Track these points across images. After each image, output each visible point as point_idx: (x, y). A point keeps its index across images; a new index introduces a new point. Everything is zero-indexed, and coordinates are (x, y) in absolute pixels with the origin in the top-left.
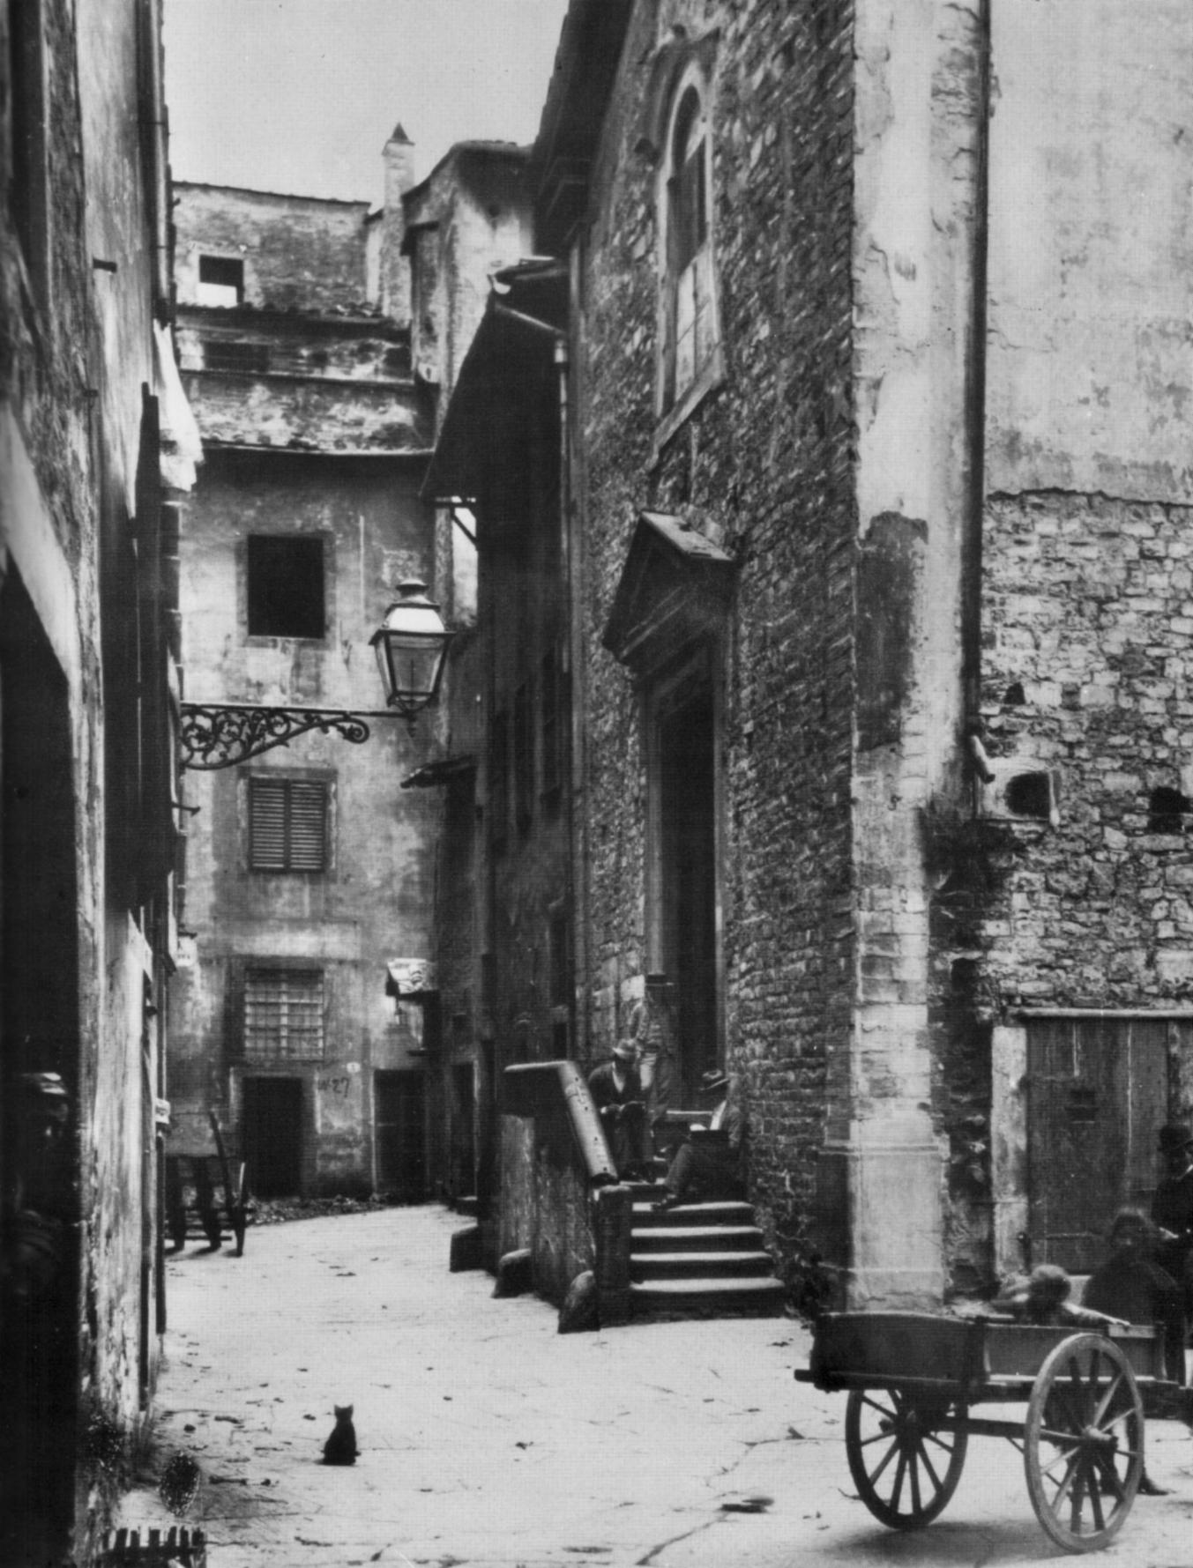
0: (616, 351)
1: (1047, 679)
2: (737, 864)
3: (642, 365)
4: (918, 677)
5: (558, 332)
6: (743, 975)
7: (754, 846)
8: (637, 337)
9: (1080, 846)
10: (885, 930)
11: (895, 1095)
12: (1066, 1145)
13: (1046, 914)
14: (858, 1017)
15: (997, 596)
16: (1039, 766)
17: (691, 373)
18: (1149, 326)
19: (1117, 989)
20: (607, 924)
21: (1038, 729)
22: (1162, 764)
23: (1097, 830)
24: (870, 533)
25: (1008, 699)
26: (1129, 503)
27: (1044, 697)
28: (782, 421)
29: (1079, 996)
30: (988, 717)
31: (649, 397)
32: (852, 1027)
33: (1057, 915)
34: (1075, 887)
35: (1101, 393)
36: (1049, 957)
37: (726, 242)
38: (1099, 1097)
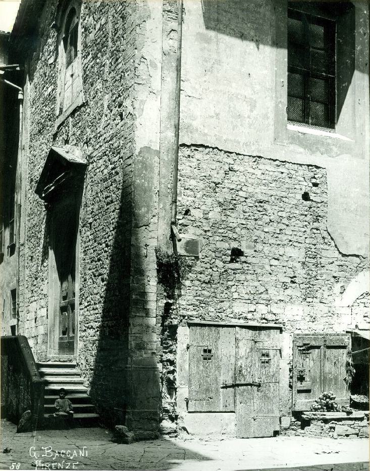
0: (41, 94)
1: (199, 208)
2: (84, 268)
3: (52, 99)
4: (279, 49)
5: (20, 88)
6: (86, 307)
7: (92, 262)
8: (50, 90)
9: (208, 266)
10: (142, 291)
11: (144, 349)
12: (201, 368)
13: (196, 288)
14: (131, 321)
15: (182, 179)
16: (194, 237)
17: (70, 101)
18: (233, 95)
19: (219, 314)
20: (32, 291)
21: (195, 225)
22: (235, 239)
23: (214, 260)
24: (140, 153)
25: (185, 214)
26: (226, 152)
27: (196, 214)
28: (106, 116)
29: (207, 317)
30: (179, 219)
31: (53, 110)
32: (130, 324)
33: (200, 289)
34: (207, 279)
35: (217, 115)
36: (197, 303)
37: (85, 57)
38: (213, 352)
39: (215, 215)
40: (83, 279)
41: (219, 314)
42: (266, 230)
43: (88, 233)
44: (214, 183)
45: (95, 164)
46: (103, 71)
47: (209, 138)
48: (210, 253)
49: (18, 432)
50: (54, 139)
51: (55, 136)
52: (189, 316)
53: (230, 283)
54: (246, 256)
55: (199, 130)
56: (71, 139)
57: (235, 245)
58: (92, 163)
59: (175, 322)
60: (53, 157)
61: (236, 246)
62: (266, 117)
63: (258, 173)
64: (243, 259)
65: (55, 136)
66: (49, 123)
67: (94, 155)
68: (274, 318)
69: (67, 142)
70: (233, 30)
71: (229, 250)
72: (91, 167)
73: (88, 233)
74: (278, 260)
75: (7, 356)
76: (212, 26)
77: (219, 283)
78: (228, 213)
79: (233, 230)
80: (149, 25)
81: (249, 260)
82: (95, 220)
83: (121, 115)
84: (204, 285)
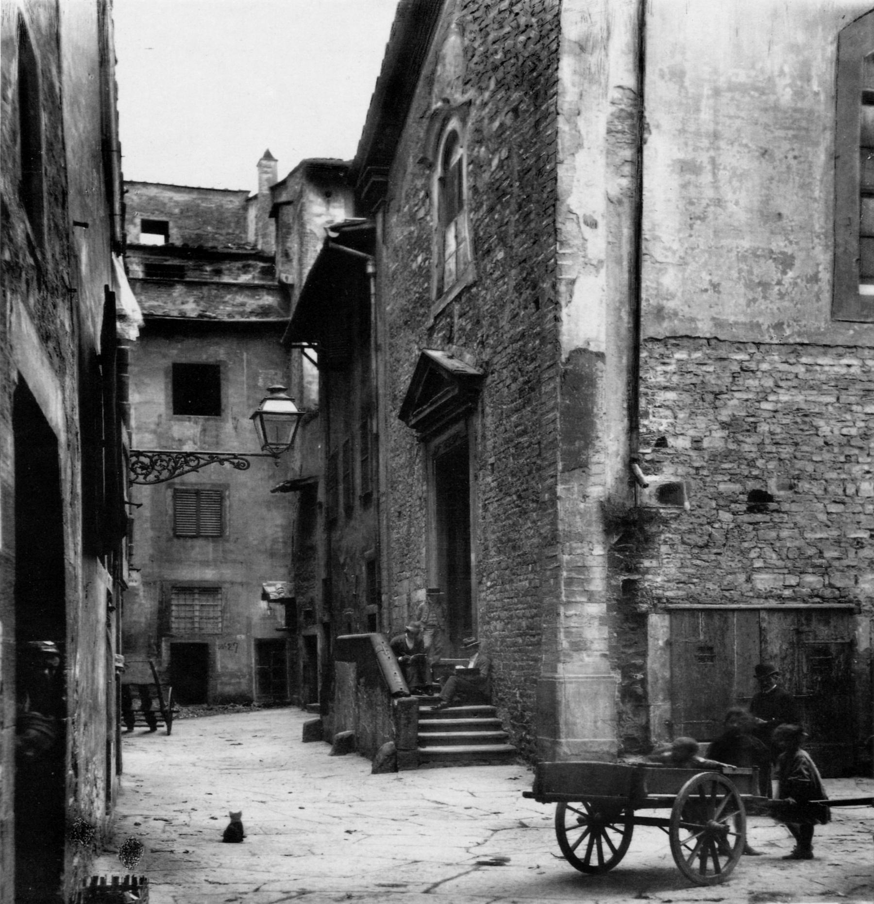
0: (406, 266)
3: (424, 273)
9: (703, 520)
16: (673, 479)
22: (756, 477)
24: (568, 359)
25: (657, 445)
28: (513, 302)
31: (428, 290)
32: (558, 614)
36: (684, 578)
37: (476, 210)
38: (716, 650)
39: (716, 440)
40: (482, 547)
41: (727, 594)
42: (816, 458)
43: (489, 479)
44: (712, 392)
45: (496, 375)
46: (506, 231)
47: (700, 325)
48: (706, 500)
49: (374, 772)
50: (430, 335)
51: (431, 330)
52: (669, 600)
53: (746, 545)
54: (779, 502)
55: (680, 314)
56: (457, 336)
57: (751, 485)
58: (492, 373)
59: (644, 607)
60: (426, 363)
61: (758, 487)
62: (814, 279)
63: (801, 370)
64: (772, 506)
65: (431, 330)
66: (422, 311)
67: (495, 360)
68: (392, 896)
69: (449, 340)
70: (746, 146)
71: (743, 493)
72: (489, 380)
73: (489, 479)
74: (844, 503)
75: (354, 664)
76: (702, 145)
77: (724, 545)
78: (741, 438)
79: (751, 463)
80: (581, 158)
81: (786, 507)
82: (500, 460)
83: (537, 302)
84: (696, 551)
